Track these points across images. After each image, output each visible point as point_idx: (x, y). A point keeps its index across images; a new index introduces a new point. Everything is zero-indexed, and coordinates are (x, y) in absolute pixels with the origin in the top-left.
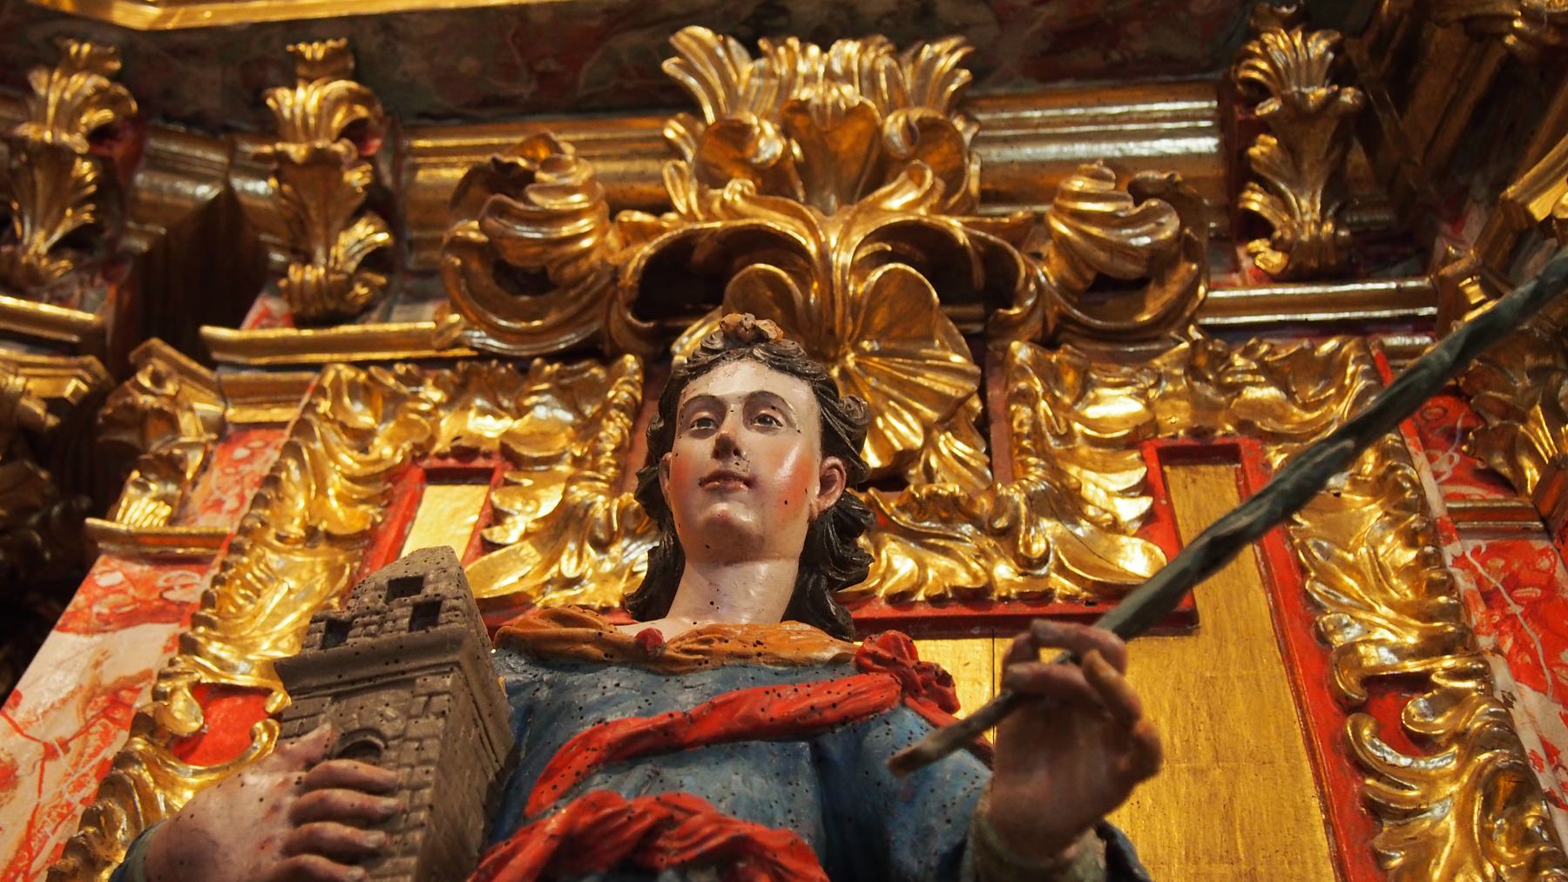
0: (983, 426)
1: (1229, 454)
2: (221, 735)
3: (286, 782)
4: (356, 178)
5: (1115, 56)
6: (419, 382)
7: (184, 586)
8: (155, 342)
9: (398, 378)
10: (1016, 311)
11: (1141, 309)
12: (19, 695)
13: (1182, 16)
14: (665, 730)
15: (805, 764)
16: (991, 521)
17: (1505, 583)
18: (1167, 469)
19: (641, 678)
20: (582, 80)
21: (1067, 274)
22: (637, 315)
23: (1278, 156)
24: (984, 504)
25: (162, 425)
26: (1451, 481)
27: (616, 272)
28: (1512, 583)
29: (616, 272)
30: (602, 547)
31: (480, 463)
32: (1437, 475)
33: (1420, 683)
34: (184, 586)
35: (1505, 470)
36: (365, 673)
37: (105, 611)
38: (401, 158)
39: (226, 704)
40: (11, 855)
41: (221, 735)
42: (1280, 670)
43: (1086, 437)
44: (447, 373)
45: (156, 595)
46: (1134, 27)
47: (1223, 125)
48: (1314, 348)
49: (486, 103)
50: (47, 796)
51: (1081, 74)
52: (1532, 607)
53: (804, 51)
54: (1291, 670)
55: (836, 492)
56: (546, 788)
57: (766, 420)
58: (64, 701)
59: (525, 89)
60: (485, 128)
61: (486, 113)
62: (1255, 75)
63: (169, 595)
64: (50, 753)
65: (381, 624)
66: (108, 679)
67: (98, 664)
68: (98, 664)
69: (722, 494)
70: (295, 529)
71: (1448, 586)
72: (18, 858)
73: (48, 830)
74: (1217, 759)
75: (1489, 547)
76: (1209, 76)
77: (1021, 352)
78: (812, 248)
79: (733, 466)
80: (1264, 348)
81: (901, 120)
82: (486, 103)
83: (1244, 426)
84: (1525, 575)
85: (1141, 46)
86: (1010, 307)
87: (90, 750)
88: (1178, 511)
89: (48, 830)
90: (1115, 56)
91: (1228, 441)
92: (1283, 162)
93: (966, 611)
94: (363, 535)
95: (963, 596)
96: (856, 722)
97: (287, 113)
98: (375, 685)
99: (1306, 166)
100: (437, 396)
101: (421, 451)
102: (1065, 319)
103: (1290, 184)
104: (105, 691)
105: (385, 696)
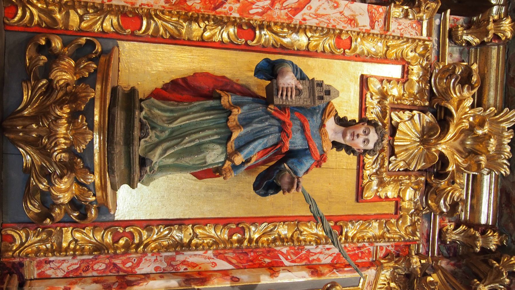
0: (406, 170)
1: (396, 213)
2: (342, 42)
3: (293, 85)
4: (485, 39)
5: (504, 206)
6: (427, 60)
7: (379, 24)
8: (440, 4)
9: (428, 56)
10: (433, 178)
11: (432, 202)
12: (353, 3)
13: (510, 221)
14: (305, 131)
15: (304, 148)
16: (379, 171)
17: (362, 252)
18: (394, 202)
19: (319, 125)
20: (512, 87)
21: (440, 189)
22: (51, 231)
23: (470, 234)
24: (383, 170)
25: (418, 10)
26: (386, 249)
27: (448, 101)
28: (362, 253)
29: (448, 101)
30: (379, 102)
31: (405, 76)
32: (388, 246)
33: (341, 234)
34: (379, 24)
35: (387, 258)
36: (311, 91)
37: (373, 12)
38: (232, 162)
39: (349, 41)
40: (320, 14)
41: (342, 42)
42: (347, 214)
43: (402, 188)
44: (429, 66)
45: (376, 20)
46: (508, 211)
47: (486, 226)
48: (418, 232)
49: (509, 65)
50: (332, 15)
51: (501, 198)
52: (357, 254)
53: (509, 139)
54: (346, 215)
55: (358, 151)
56: (299, 115)
57: (364, 142)
58: (352, 11)
59: (511, 74)
60: (504, 65)
61: (507, 65)
62: (489, 232)
63: (377, 23)
64: (341, 13)
65: (321, 91)
66: (357, 17)
67: (360, 14)
68: (360, 14)
69: (351, 135)
70: (389, 44)
71: (358, 242)
72: (320, 15)
73: (325, 18)
74: (330, 202)
75: (370, 251)
76: (497, 224)
77: (423, 179)
78: (442, 141)
79: (355, 137)
80: (419, 223)
81: (483, 160)
82: (509, 65)
83: (401, 216)
84: (364, 255)
85: (505, 211)
86: (434, 177)
87: (341, 19)
88: (383, 202)
89: (325, 18)
90: (504, 206)
91: (398, 213)
92: (468, 234)
93: (361, 165)
94: (387, 58)
95: (364, 165)
96: (311, 155)
97: (503, 22)
98: (310, 93)
99: (467, 239)
100: (424, 64)
101: (409, 63)
102: (431, 187)
103: (463, 235)
104: (354, 18)
105: (308, 94)
